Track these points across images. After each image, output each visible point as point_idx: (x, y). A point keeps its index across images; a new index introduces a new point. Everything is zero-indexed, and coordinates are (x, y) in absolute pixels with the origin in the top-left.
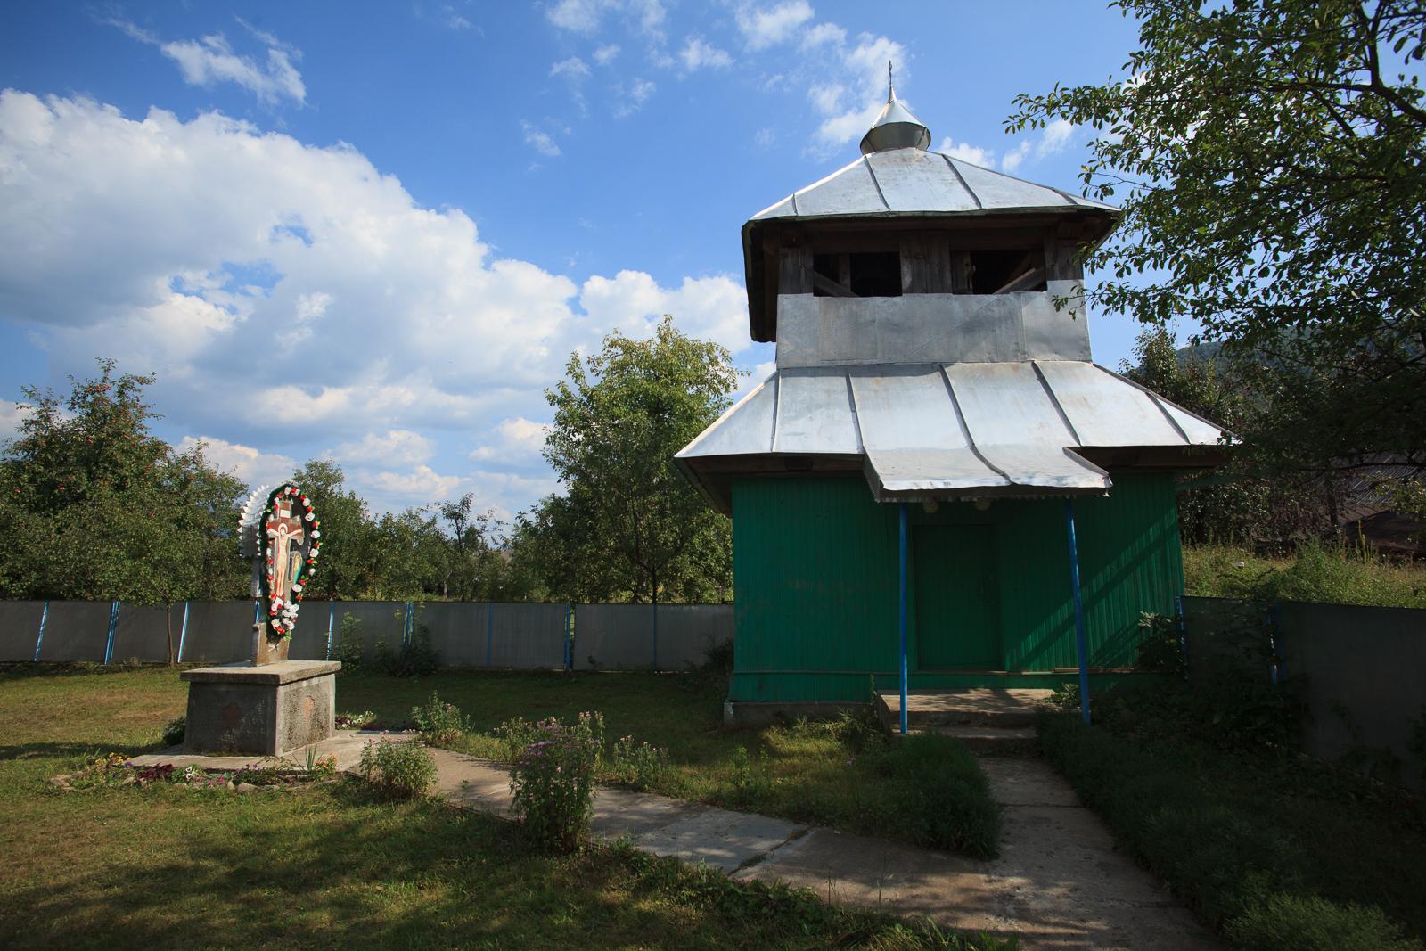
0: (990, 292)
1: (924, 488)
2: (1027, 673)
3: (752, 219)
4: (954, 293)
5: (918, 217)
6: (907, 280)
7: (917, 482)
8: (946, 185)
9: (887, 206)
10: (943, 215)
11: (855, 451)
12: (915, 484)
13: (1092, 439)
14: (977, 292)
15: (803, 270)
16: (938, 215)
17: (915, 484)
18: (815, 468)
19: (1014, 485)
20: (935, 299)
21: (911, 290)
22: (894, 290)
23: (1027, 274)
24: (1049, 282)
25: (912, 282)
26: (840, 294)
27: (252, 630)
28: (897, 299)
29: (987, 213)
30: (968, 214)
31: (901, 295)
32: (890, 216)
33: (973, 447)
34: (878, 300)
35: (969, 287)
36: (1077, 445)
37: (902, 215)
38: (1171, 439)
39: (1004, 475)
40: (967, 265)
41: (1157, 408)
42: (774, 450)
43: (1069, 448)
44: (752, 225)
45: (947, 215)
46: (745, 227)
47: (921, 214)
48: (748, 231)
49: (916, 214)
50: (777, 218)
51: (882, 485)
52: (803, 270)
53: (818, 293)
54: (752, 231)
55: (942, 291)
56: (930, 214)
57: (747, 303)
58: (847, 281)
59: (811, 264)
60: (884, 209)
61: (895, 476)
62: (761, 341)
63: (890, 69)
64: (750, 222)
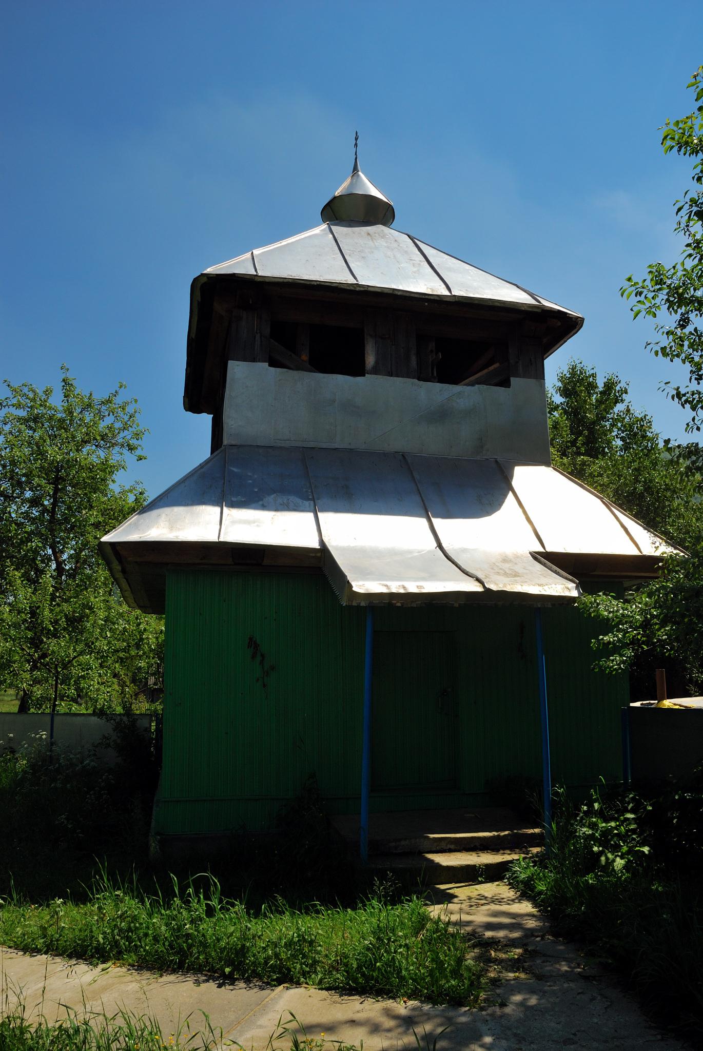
0: (456, 382)
1: (394, 590)
2: (471, 815)
3: (205, 272)
4: (419, 379)
5: (387, 294)
6: (370, 360)
7: (389, 583)
8: (414, 265)
9: (355, 278)
10: (413, 295)
11: (316, 545)
12: (386, 586)
13: (553, 546)
14: (441, 381)
15: (258, 337)
16: (408, 294)
17: (386, 586)
18: (266, 562)
19: (488, 591)
20: (398, 382)
21: (375, 371)
22: (357, 369)
23: (491, 368)
24: (512, 379)
25: (377, 362)
26: (298, 368)
27: (23, 717)
28: (359, 379)
29: (457, 300)
30: (438, 298)
31: (364, 375)
32: (358, 289)
33: (440, 546)
34: (340, 377)
35: (433, 374)
36: (542, 550)
37: (370, 289)
38: (630, 550)
39: (478, 580)
40: (432, 351)
41: (629, 519)
42: (221, 539)
43: (535, 552)
44: (205, 279)
45: (416, 296)
46: (195, 280)
47: (391, 292)
48: (199, 285)
49: (386, 291)
50: (234, 275)
51: (351, 587)
52: (258, 337)
53: (273, 363)
54: (203, 286)
55: (408, 376)
56: (399, 293)
57: (185, 367)
58: (305, 357)
59: (267, 331)
60: (351, 280)
61: (366, 574)
62: (194, 412)
63: (356, 139)
64: (202, 274)
